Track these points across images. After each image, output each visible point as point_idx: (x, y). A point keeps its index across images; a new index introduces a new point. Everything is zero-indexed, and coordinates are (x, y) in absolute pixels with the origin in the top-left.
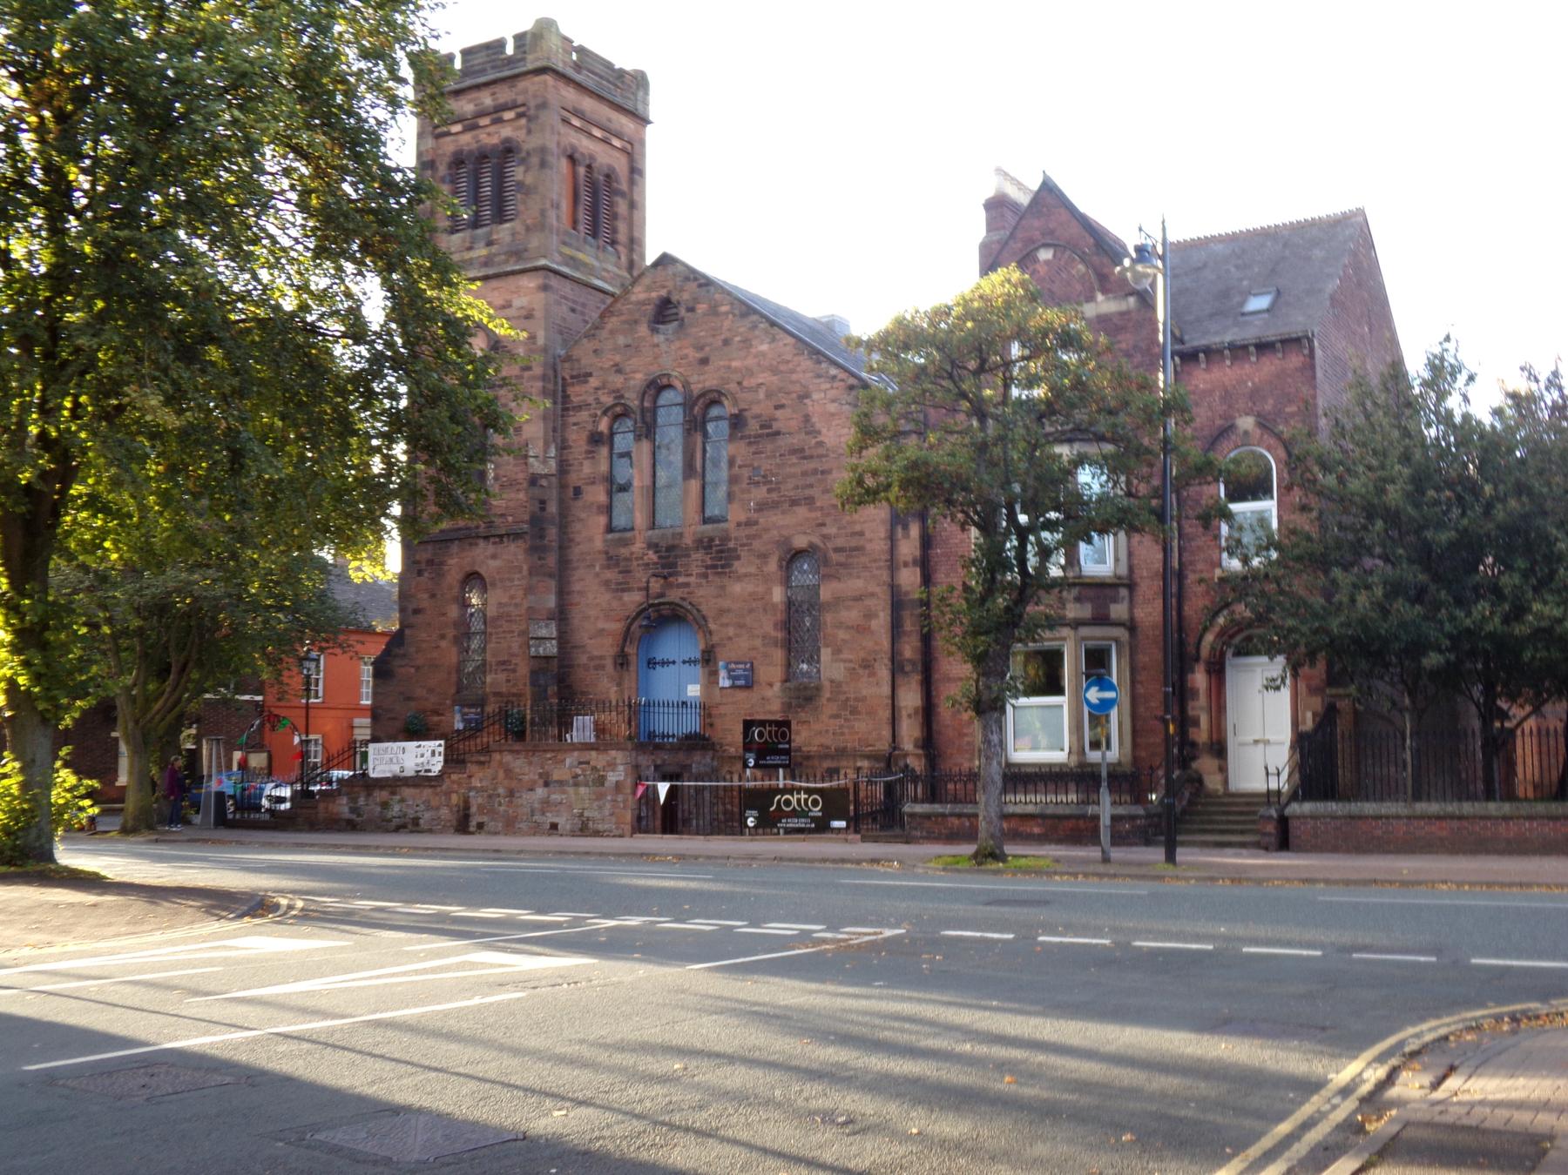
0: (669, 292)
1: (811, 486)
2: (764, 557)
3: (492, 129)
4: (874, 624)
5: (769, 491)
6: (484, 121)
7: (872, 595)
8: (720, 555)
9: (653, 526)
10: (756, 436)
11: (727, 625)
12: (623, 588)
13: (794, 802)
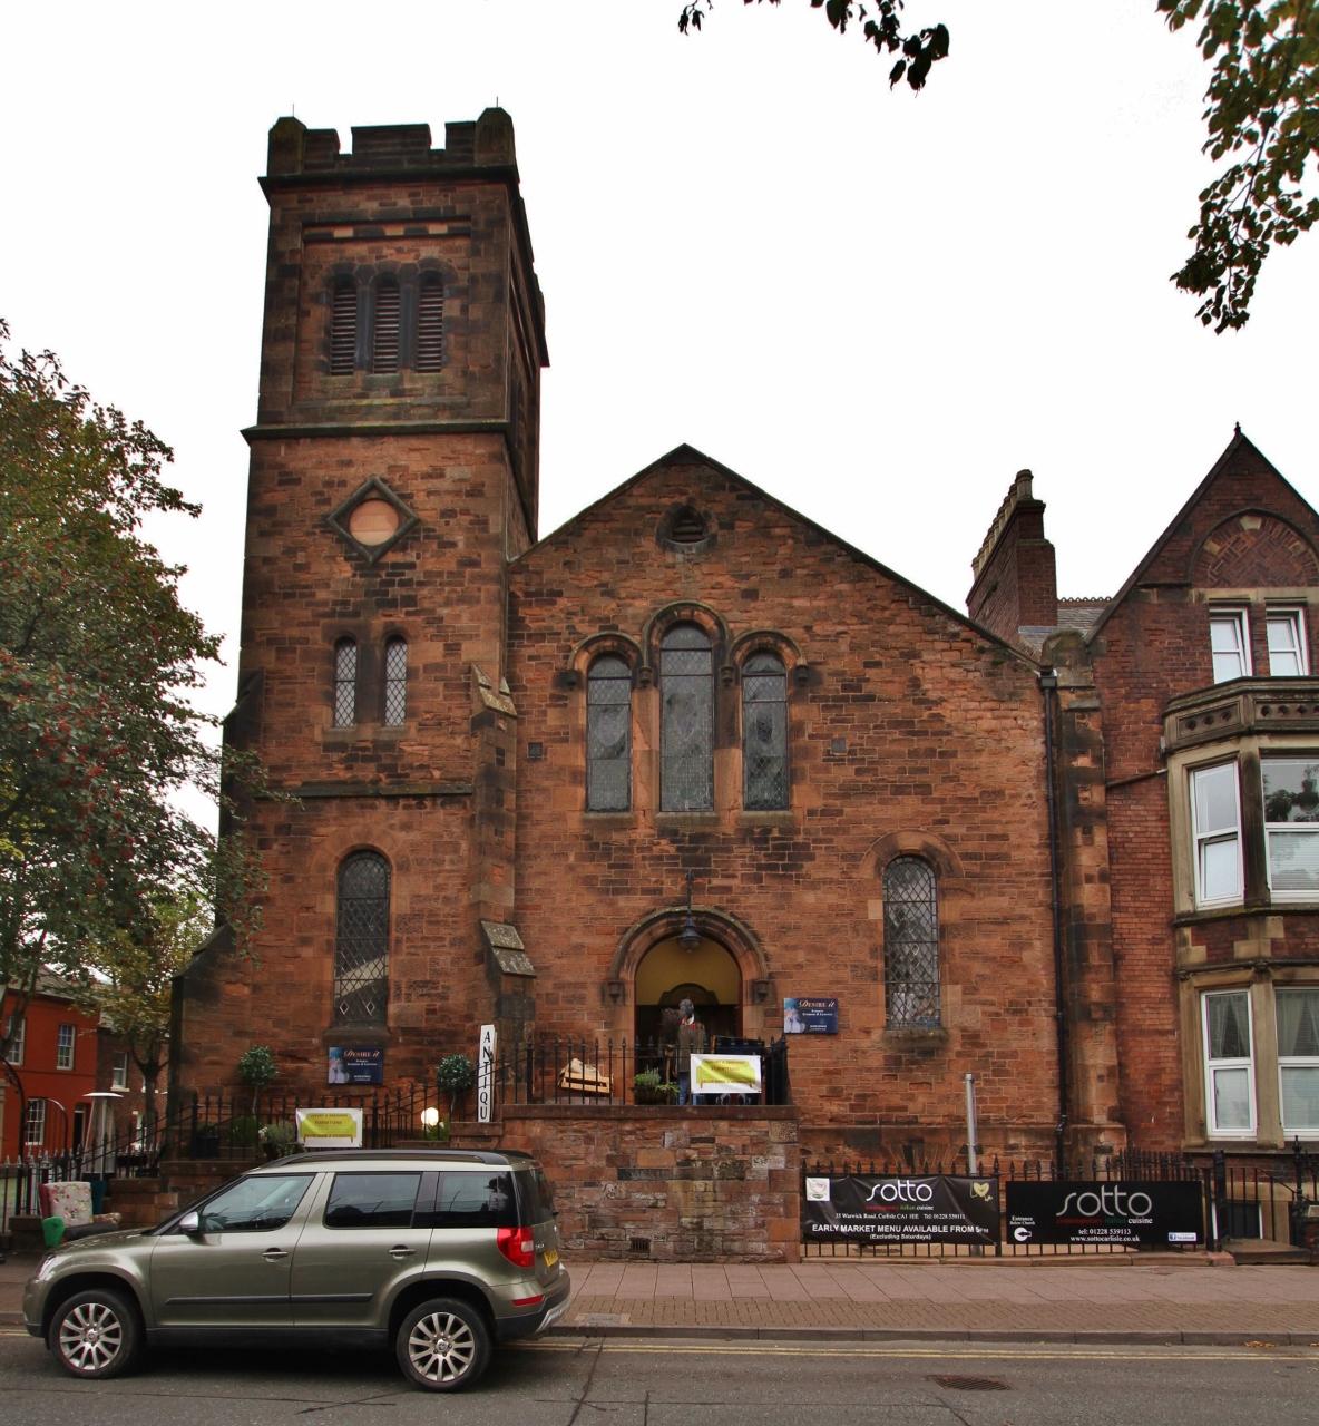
0: (691, 500)
1: (924, 770)
2: (853, 858)
4: (1027, 956)
5: (858, 772)
7: (1023, 918)
10: (835, 699)
11: (795, 948)
13: (1101, 1205)
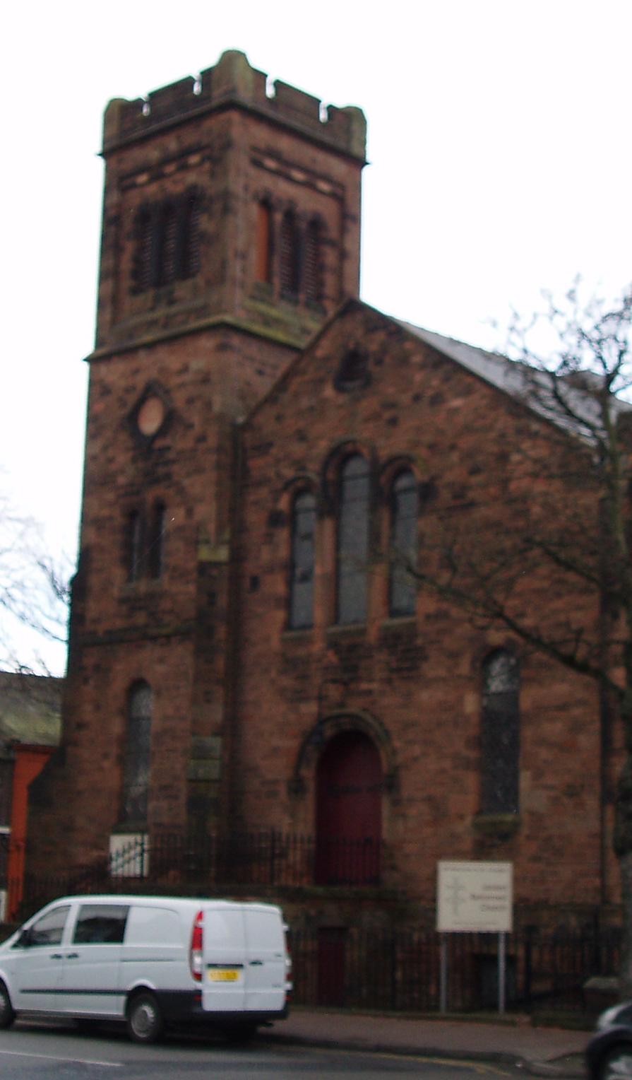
2: (454, 655)
3: (178, 176)
6: (170, 169)
8: (405, 652)
9: (335, 618)
12: (299, 697)
